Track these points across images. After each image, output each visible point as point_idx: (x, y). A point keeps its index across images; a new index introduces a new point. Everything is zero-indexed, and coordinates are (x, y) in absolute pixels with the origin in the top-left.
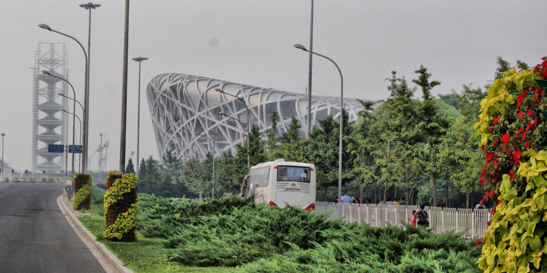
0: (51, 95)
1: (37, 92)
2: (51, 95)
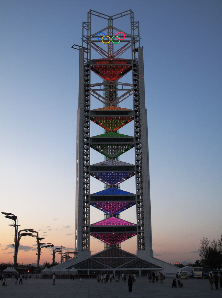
0: (111, 95)
1: (86, 90)
2: (111, 95)
